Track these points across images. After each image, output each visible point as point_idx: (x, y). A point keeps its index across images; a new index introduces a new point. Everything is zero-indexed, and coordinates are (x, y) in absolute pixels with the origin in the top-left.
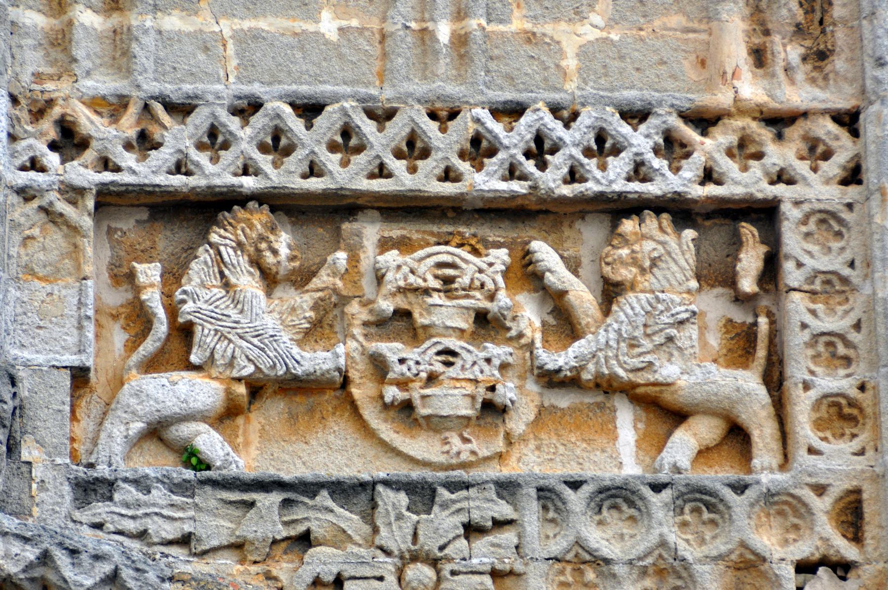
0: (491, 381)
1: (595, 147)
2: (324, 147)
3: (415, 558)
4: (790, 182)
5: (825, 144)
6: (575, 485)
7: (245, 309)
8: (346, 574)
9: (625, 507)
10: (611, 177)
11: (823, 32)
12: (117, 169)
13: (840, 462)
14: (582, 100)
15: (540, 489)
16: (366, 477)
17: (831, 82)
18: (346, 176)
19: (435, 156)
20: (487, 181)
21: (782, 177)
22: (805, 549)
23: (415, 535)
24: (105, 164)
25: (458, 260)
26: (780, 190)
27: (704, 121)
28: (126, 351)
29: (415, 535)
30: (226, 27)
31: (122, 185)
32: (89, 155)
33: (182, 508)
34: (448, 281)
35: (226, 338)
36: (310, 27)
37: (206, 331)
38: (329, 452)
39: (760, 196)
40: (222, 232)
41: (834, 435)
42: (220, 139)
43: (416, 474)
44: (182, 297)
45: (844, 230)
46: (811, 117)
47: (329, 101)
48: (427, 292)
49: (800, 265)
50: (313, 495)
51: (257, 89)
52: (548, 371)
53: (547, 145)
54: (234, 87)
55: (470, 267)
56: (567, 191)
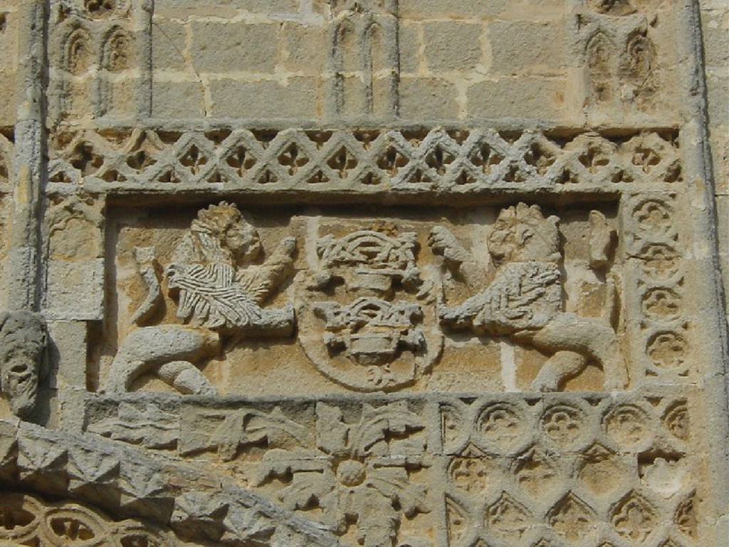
0: (403, 328)
1: (482, 158)
2: (277, 162)
3: (347, 456)
4: (629, 180)
5: (654, 153)
6: (468, 401)
7: (211, 273)
8: (294, 468)
9: (507, 416)
10: (490, 178)
11: (651, 74)
12: (123, 179)
13: (672, 381)
14: (471, 124)
15: (442, 404)
16: (309, 397)
17: (657, 109)
18: (290, 180)
19: (360, 166)
20: (392, 181)
21: (619, 177)
22: (643, 445)
23: (346, 439)
24: (112, 175)
25: (379, 241)
26: (621, 186)
27: (562, 137)
28: (129, 311)
29: (346, 439)
30: (205, 78)
31: (126, 190)
32: (102, 170)
33: (168, 421)
34: (372, 255)
35: (204, 298)
36: (269, 77)
37: (188, 294)
38: (284, 377)
39: (606, 190)
40: (200, 223)
41: (665, 362)
42: (200, 156)
43: (347, 394)
44: (170, 270)
45: (670, 214)
46: (642, 134)
47: (279, 128)
48: (353, 264)
49: (636, 238)
50: (271, 409)
51: (226, 120)
52: (448, 319)
53: (445, 155)
54: (208, 122)
55: (386, 245)
56: (559, 188)
